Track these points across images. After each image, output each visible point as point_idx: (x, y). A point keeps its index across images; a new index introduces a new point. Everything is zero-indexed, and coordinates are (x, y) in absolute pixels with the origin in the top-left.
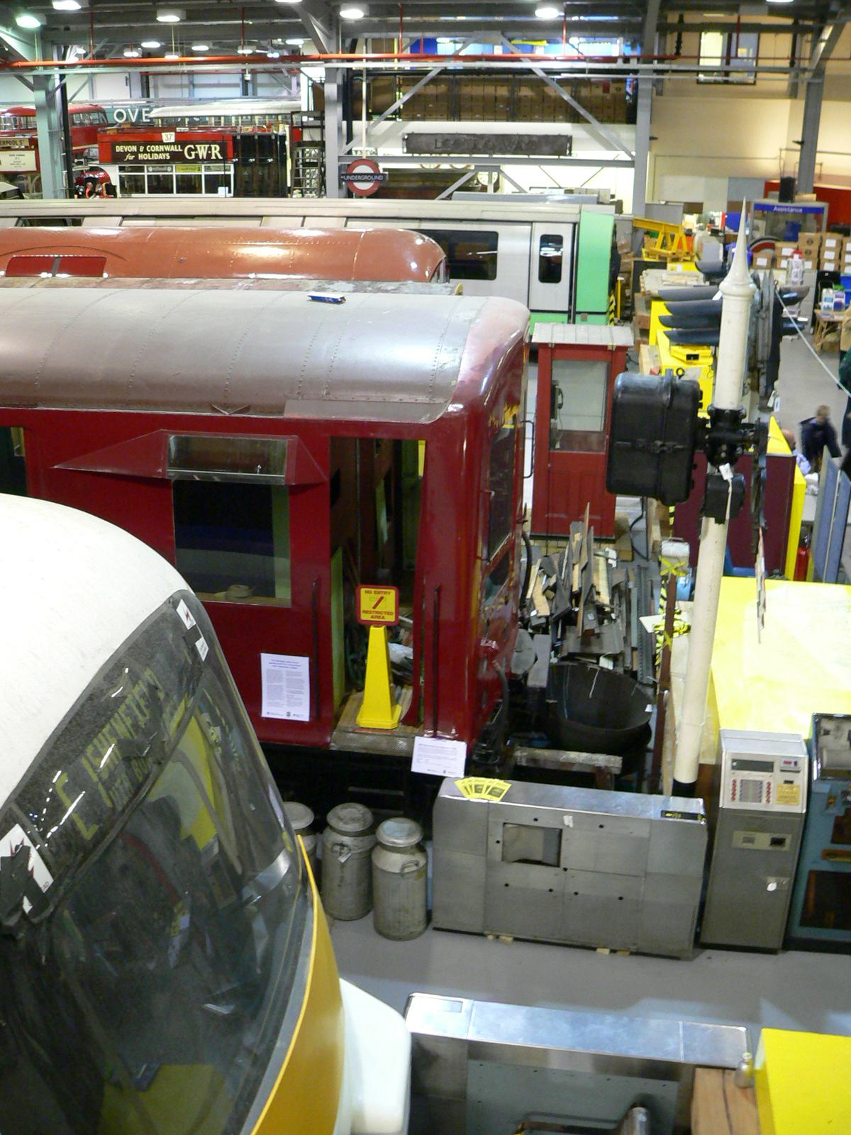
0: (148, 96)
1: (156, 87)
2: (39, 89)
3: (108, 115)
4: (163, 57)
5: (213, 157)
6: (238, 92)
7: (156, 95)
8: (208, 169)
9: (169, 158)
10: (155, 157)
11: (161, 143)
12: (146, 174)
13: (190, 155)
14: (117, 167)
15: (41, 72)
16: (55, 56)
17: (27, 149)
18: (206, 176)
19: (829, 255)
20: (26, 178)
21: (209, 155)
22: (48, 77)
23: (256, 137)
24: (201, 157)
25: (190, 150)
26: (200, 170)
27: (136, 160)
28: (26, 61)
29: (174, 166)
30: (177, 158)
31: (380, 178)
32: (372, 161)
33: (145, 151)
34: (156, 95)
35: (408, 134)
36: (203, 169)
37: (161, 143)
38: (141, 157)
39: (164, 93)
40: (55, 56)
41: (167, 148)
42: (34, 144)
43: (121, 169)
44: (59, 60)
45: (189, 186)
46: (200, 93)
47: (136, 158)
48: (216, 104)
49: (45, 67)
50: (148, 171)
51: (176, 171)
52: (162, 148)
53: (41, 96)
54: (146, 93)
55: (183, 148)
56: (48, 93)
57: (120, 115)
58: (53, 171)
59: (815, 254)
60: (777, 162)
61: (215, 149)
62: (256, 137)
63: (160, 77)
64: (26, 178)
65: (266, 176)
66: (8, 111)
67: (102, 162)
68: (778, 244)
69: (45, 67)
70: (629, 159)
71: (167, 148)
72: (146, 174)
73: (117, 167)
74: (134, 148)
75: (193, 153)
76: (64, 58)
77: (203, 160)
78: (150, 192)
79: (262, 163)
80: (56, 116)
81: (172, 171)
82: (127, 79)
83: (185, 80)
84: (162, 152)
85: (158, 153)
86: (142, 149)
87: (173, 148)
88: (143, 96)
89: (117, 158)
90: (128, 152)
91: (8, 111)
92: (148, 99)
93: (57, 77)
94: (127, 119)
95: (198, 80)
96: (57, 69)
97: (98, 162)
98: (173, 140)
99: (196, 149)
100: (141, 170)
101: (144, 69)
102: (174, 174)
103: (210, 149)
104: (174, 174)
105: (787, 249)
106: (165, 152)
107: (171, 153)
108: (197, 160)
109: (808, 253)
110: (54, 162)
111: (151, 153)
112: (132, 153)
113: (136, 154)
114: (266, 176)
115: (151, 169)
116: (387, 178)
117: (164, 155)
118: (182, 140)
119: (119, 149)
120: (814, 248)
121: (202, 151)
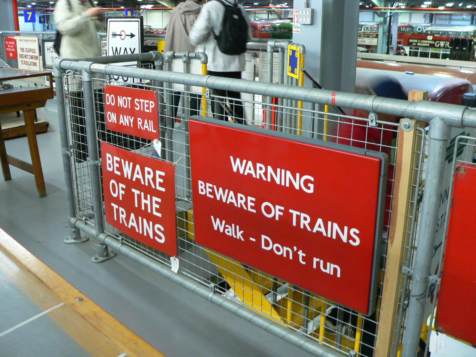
0: (432, 22)
1: (435, 19)
2: (382, 17)
3: (414, 29)
4: (438, 8)
5: (446, 47)
6: (469, 23)
7: (435, 22)
8: (443, 51)
9: (429, 45)
10: (424, 45)
11: (427, 40)
12: (419, 51)
13: (437, 45)
14: (408, 48)
15: (383, 11)
16: (389, 6)
17: (375, 37)
18: (442, 54)
20: (373, 48)
21: (444, 46)
22: (385, 13)
23: (460, 40)
24: (441, 46)
25: (437, 43)
26: (440, 51)
27: (416, 45)
28: (378, 7)
29: (430, 49)
30: (432, 46)
33: (420, 42)
34: (435, 22)
36: (441, 51)
37: (427, 40)
38: (418, 44)
39: (438, 22)
40: (389, 6)
41: (429, 42)
42: (377, 36)
43: (410, 48)
44: (391, 7)
46: (453, 23)
47: (417, 44)
48: (457, 27)
49: (385, 9)
50: (420, 50)
51: (431, 51)
52: (427, 42)
53: (382, 19)
54: (431, 21)
55: (435, 42)
56: (384, 18)
57: (419, 29)
58: (382, 45)
61: (447, 43)
62: (460, 40)
63: (438, 15)
64: (373, 48)
65: (463, 54)
66: (376, 25)
69: (385, 9)
71: (429, 42)
72: (419, 51)
73: (408, 48)
74: (416, 41)
75: (438, 45)
76: (392, 6)
77: (442, 48)
79: (461, 50)
80: (386, 27)
81: (429, 50)
82: (424, 15)
83: (448, 17)
84: (426, 43)
85: (425, 43)
86: (419, 41)
87: (431, 42)
88: (430, 22)
89: (409, 44)
90: (414, 42)
91: (376, 25)
92: (431, 24)
93: (389, 13)
94: (422, 31)
95: (453, 17)
96: (389, 10)
97: (402, 45)
98: (431, 39)
99: (440, 43)
101: (430, 12)
102: (430, 52)
104: (430, 52)
106: (428, 43)
108: (440, 47)
110: (383, 43)
111: (422, 43)
112: (415, 43)
113: (417, 43)
114: (463, 54)
117: (427, 44)
118: (435, 39)
119: (411, 41)
121: (442, 44)
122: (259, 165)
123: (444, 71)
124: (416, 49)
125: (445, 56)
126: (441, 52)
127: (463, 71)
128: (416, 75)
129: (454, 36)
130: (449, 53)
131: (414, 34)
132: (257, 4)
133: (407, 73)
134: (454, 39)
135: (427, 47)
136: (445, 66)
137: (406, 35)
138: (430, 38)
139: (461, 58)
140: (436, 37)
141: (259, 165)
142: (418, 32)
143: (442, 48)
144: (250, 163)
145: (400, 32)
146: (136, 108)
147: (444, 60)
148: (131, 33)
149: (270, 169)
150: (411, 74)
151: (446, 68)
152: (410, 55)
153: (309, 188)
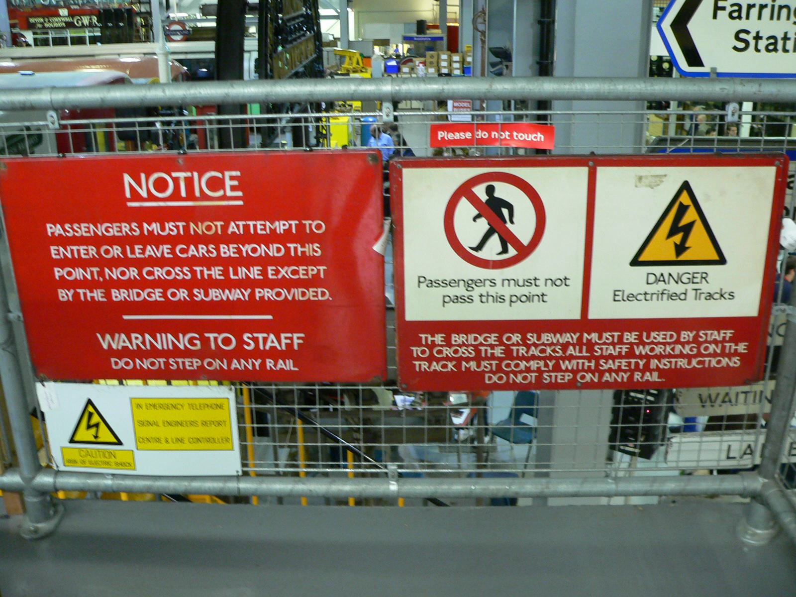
10: (56, 25)
11: (59, 16)
19: (444, 64)
26: (85, 32)
27: (44, 27)
30: (70, 25)
31: (186, 32)
32: (181, 22)
35: (203, 5)
43: (34, 33)
45: (79, 41)
59: (435, 64)
60: (431, 13)
67: (21, 28)
68: (414, 59)
70: (337, 14)
71: (63, 19)
74: (41, 20)
75: (80, 22)
77: (87, 27)
78: (54, 44)
87: (68, 20)
89: (31, 27)
100: (47, 33)
103: (91, 19)
105: (417, 61)
107: (66, 23)
109: (431, 63)
112: (41, 23)
115: (53, 33)
116: (191, 32)
118: (72, 14)
119: (32, 20)
120: (434, 60)
121: (86, 20)
122: (133, 335)
123: (94, 63)
124: (44, 33)
125: (94, 40)
126: (87, 34)
127: (125, 59)
128: (38, 75)
129: (102, 6)
130: (99, 34)
131: (36, 9)
132: (280, 63)
133: (22, 74)
134: (102, 11)
135: (62, 28)
136: (93, 56)
137: (23, 12)
138: (64, 12)
139: (119, 40)
140: (74, 10)
141: (133, 335)
142: (43, 5)
143: (87, 27)
144: (123, 336)
145: (12, 8)
146: (246, 347)
147: (93, 47)
148: (688, 248)
149: (147, 337)
150: (30, 75)
151: (97, 58)
152: (36, 45)
153: (195, 345)
